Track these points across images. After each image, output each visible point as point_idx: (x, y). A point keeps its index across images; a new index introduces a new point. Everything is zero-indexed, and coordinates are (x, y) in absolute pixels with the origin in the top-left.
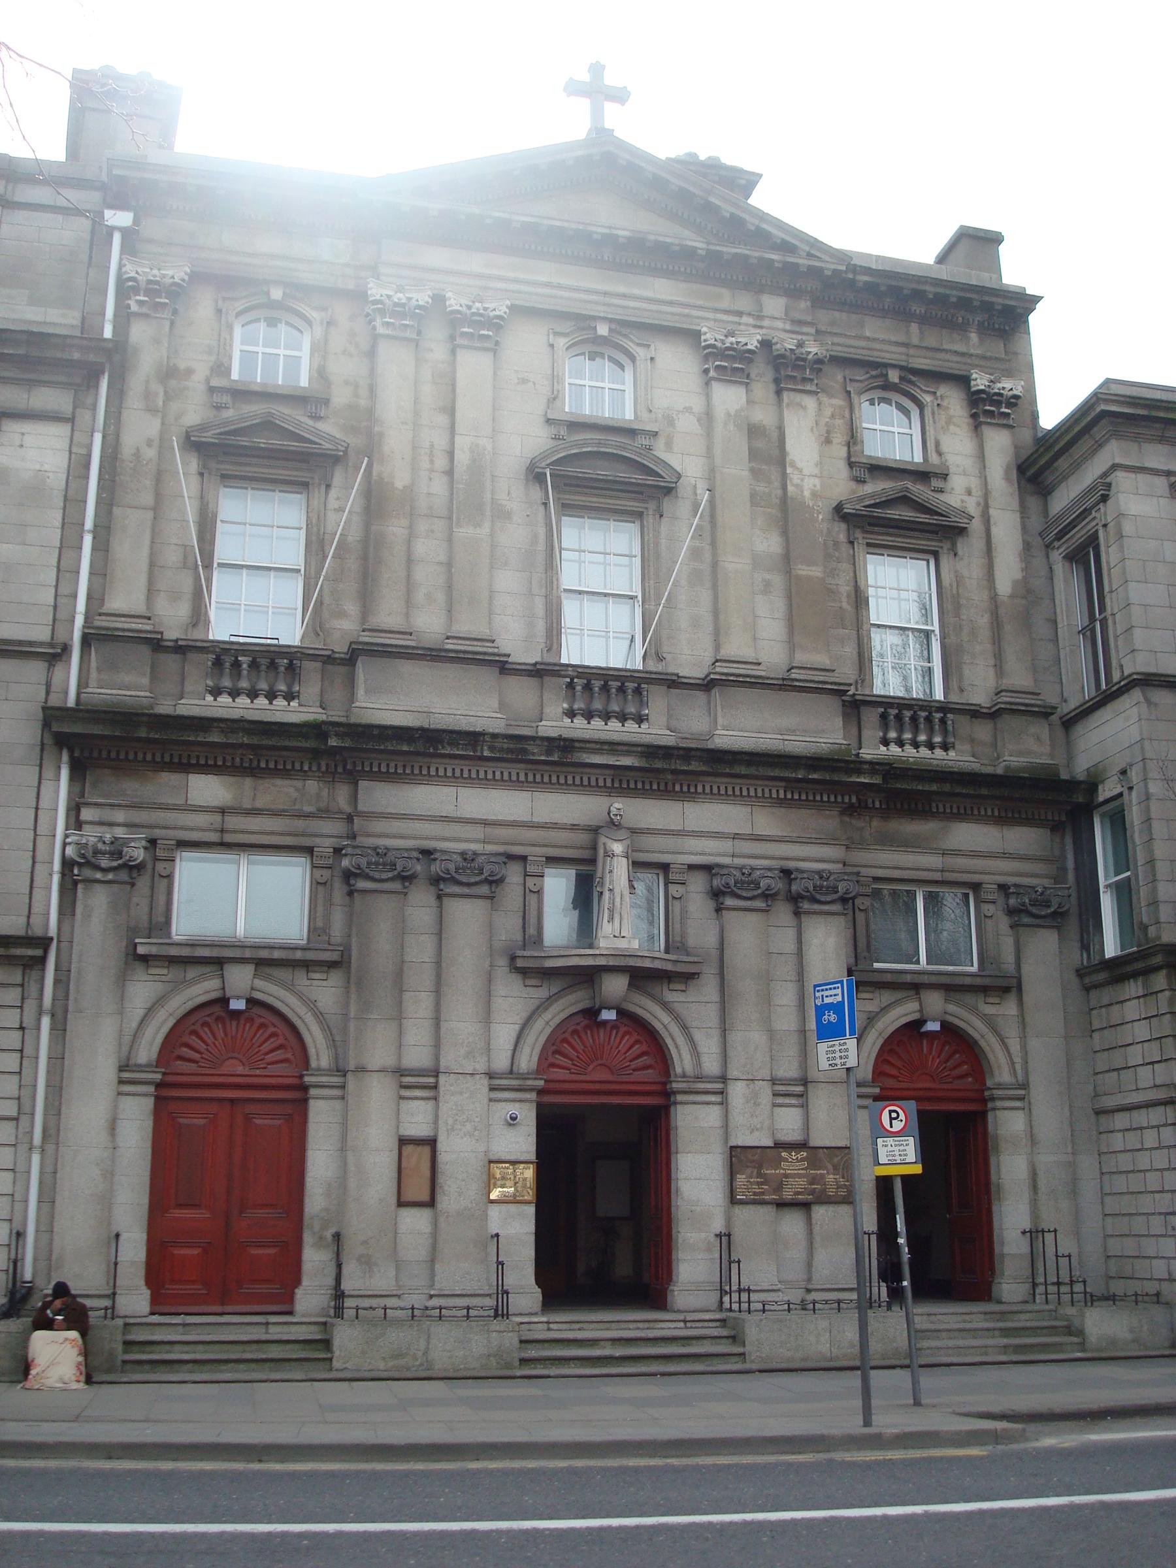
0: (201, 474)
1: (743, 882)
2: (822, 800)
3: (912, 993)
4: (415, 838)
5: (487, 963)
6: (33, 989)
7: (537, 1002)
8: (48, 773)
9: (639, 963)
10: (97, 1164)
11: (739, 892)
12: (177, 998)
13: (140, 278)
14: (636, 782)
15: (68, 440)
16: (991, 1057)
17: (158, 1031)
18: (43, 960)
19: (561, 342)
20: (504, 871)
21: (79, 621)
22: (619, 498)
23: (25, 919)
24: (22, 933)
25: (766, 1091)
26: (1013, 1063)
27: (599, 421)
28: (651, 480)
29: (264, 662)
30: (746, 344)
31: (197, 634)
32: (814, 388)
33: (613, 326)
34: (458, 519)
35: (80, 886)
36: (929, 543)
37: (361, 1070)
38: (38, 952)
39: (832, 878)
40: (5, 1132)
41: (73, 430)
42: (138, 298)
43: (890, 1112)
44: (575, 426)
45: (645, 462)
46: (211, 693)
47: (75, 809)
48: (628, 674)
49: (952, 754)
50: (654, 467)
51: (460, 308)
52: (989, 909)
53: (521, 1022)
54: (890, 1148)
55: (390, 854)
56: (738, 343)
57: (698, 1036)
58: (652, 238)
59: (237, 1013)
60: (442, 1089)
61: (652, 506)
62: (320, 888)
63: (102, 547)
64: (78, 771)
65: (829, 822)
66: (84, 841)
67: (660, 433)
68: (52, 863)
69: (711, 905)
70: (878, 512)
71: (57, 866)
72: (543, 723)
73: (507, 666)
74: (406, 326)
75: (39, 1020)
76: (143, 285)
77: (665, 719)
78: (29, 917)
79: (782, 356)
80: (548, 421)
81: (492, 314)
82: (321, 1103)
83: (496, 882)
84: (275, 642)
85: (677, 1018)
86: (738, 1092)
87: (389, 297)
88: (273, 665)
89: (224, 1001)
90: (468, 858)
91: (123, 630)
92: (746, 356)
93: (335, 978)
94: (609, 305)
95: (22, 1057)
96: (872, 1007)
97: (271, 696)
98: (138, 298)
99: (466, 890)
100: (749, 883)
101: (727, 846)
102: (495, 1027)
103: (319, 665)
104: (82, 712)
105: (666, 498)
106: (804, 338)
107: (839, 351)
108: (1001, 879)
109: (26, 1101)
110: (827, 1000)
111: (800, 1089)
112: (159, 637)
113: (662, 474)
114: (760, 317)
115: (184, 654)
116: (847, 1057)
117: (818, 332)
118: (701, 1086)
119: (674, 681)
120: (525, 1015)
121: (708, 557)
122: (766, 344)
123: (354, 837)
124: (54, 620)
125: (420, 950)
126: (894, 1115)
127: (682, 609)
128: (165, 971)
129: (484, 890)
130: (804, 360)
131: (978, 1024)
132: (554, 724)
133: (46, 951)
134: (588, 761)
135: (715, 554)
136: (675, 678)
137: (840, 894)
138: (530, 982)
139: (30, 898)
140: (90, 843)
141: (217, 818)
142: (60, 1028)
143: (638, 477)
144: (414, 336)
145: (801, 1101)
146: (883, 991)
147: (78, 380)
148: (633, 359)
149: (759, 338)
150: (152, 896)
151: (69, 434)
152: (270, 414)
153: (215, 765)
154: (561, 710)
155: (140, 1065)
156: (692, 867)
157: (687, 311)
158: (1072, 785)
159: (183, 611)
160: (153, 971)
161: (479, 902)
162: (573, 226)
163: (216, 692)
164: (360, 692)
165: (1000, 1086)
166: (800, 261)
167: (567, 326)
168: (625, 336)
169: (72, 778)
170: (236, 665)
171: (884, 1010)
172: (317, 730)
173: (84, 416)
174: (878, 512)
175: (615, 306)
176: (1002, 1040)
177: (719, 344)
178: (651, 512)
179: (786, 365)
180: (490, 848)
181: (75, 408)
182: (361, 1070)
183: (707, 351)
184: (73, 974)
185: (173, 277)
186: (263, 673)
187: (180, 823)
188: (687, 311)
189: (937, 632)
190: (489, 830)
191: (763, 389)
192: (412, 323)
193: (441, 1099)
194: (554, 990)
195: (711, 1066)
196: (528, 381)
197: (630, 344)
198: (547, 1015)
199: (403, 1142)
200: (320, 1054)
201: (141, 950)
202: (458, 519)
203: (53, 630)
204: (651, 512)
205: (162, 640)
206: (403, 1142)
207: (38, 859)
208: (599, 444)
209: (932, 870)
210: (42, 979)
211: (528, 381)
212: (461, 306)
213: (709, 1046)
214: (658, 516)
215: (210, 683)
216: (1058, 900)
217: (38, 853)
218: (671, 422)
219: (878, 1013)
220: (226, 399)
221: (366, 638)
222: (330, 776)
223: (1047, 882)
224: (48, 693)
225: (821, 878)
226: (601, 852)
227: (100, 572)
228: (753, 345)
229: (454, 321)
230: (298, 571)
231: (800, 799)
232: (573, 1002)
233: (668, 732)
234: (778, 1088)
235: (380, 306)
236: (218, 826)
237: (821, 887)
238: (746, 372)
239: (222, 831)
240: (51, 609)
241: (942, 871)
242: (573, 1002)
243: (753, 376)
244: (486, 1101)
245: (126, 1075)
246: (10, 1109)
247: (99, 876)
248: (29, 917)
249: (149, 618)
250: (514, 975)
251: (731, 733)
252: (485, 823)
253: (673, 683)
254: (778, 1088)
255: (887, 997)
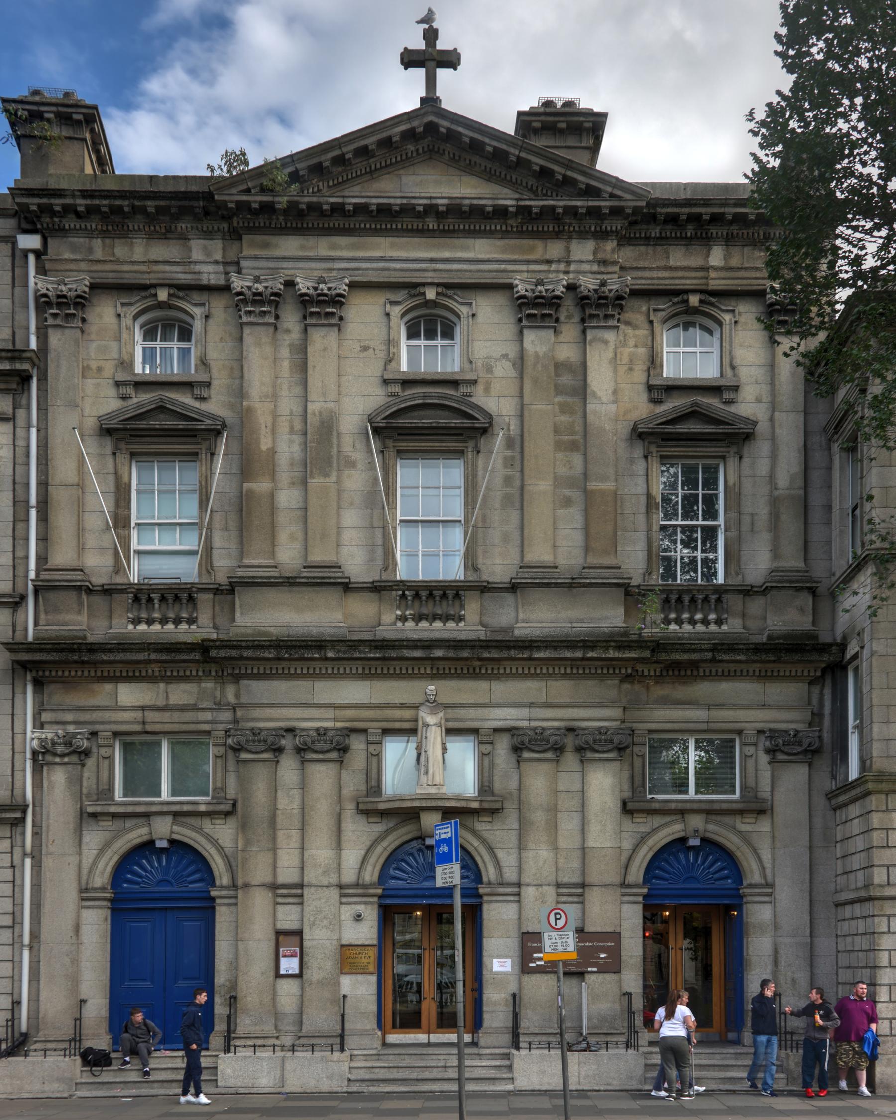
0: (114, 454)
1: (536, 740)
2: (584, 673)
3: (679, 817)
4: (282, 720)
5: (338, 808)
6: (19, 839)
7: (378, 834)
8: (19, 690)
9: (448, 804)
10: (67, 955)
11: (533, 747)
12: (120, 841)
13: (50, 294)
14: (407, 669)
15: (11, 435)
16: (745, 864)
17: (107, 864)
18: (23, 820)
19: (396, 311)
20: (347, 742)
21: (32, 575)
22: (442, 441)
23: (10, 793)
24: (9, 802)
25: (550, 891)
26: (764, 868)
27: (417, 377)
28: (467, 423)
29: (424, 594)
30: (553, 291)
31: (119, 580)
32: (615, 323)
33: (440, 290)
34: (311, 472)
35: (45, 768)
36: (717, 450)
37: (247, 885)
38: (18, 815)
39: (609, 733)
40: (6, 936)
41: (15, 427)
42: (52, 311)
43: (556, 914)
44: (407, 383)
45: (463, 408)
46: (133, 623)
47: (37, 714)
48: (447, 584)
49: (725, 627)
50: (471, 412)
51: (308, 291)
52: (750, 750)
53: (366, 848)
54: (553, 941)
55: (263, 733)
56: (546, 290)
57: (500, 854)
58: (467, 202)
59: (163, 850)
60: (305, 896)
61: (471, 444)
62: (219, 760)
63: (44, 518)
64: (39, 684)
65: (610, 689)
66: (44, 736)
67: (479, 380)
68: (25, 752)
69: (513, 759)
70: (670, 428)
71: (29, 755)
72: (381, 628)
73: (351, 586)
74: (265, 312)
75: (23, 861)
76: (54, 300)
77: (478, 618)
78: (13, 791)
79: (586, 297)
80: (386, 382)
81: (334, 292)
82: (224, 909)
83: (344, 750)
84: (178, 581)
85: (484, 841)
86: (529, 893)
87: (249, 288)
88: (177, 598)
89: (151, 842)
90: (321, 733)
91: (59, 581)
92: (554, 302)
93: (232, 823)
94: (435, 270)
95: (14, 886)
96: (644, 829)
97: (177, 621)
98: (52, 311)
99: (321, 756)
100: (541, 740)
101: (525, 713)
102: (344, 853)
103: (211, 596)
104: (39, 645)
105: (484, 436)
106: (605, 277)
107: (641, 284)
108: (760, 726)
109: (18, 914)
110: (443, 836)
111: (580, 890)
112: (348, 581)
113: (477, 416)
114: (569, 263)
115: (110, 595)
116: (453, 877)
117: (622, 268)
118: (501, 890)
119: (485, 587)
120: (369, 843)
121: (517, 483)
122: (572, 288)
123: (238, 722)
124: (14, 576)
125: (288, 802)
126: (558, 916)
127: (494, 528)
128: (110, 823)
129: (334, 755)
130: (606, 298)
131: (735, 839)
132: (390, 628)
133: (25, 812)
134: (408, 655)
135: (522, 480)
136: (485, 584)
137: (615, 745)
138: (371, 820)
139: (13, 778)
140: (49, 737)
141: (139, 715)
142: (37, 867)
143: (456, 422)
144: (272, 320)
145: (581, 899)
146: (654, 816)
147: (14, 386)
148: (720, 323)
149: (565, 283)
150: (98, 772)
151: (12, 431)
152: (162, 400)
153: (134, 676)
154: (394, 617)
155: (96, 888)
156: (496, 730)
157: (503, 266)
158: (824, 648)
159: (108, 561)
160: (101, 823)
161: (331, 765)
162: (399, 201)
163: (136, 621)
164: (238, 614)
165: (751, 886)
166: (603, 203)
167: (401, 295)
168: (450, 297)
169: (35, 692)
170: (150, 600)
171: (654, 831)
172: (204, 647)
173: (21, 413)
174: (670, 428)
175: (441, 271)
176: (755, 851)
177: (528, 294)
178: (470, 450)
179: (590, 305)
180: (339, 725)
181: (14, 408)
182: (247, 885)
183: (519, 301)
184: (44, 828)
185: (76, 290)
186: (184, 606)
187: (113, 719)
188: (503, 266)
189: (722, 526)
190: (337, 712)
191: (570, 331)
192: (269, 309)
193: (305, 904)
194: (391, 825)
195: (510, 875)
196: (369, 348)
197: (455, 303)
198: (385, 844)
199: (279, 933)
200: (223, 878)
201: (90, 810)
202: (311, 472)
203: (14, 584)
204: (470, 450)
205: (351, 583)
206: (279, 933)
207: (16, 750)
208: (424, 397)
209: (700, 722)
210: (23, 834)
211: (369, 348)
212: (308, 288)
213: (508, 860)
214: (475, 453)
215: (399, 613)
216: (809, 740)
217: (16, 747)
218: (489, 369)
219: (649, 833)
220: (130, 390)
221: (241, 573)
222: (220, 679)
223: (800, 727)
224: (14, 631)
225: (600, 733)
226: (420, 723)
227: (44, 539)
228: (560, 290)
229: (305, 301)
230: (460, 521)
231: (578, 673)
232: (405, 832)
233: (480, 627)
234: (562, 890)
235: (241, 297)
236: (141, 720)
237: (600, 740)
238: (554, 317)
239: (144, 723)
240: (11, 568)
241: (708, 722)
242: (405, 832)
243: (562, 318)
244: (338, 905)
245: (84, 895)
246: (8, 920)
247: (57, 760)
248: (13, 791)
249: (276, 567)
250: (360, 816)
251: (528, 625)
252: (334, 707)
253: (485, 589)
254: (562, 890)
255: (657, 820)
